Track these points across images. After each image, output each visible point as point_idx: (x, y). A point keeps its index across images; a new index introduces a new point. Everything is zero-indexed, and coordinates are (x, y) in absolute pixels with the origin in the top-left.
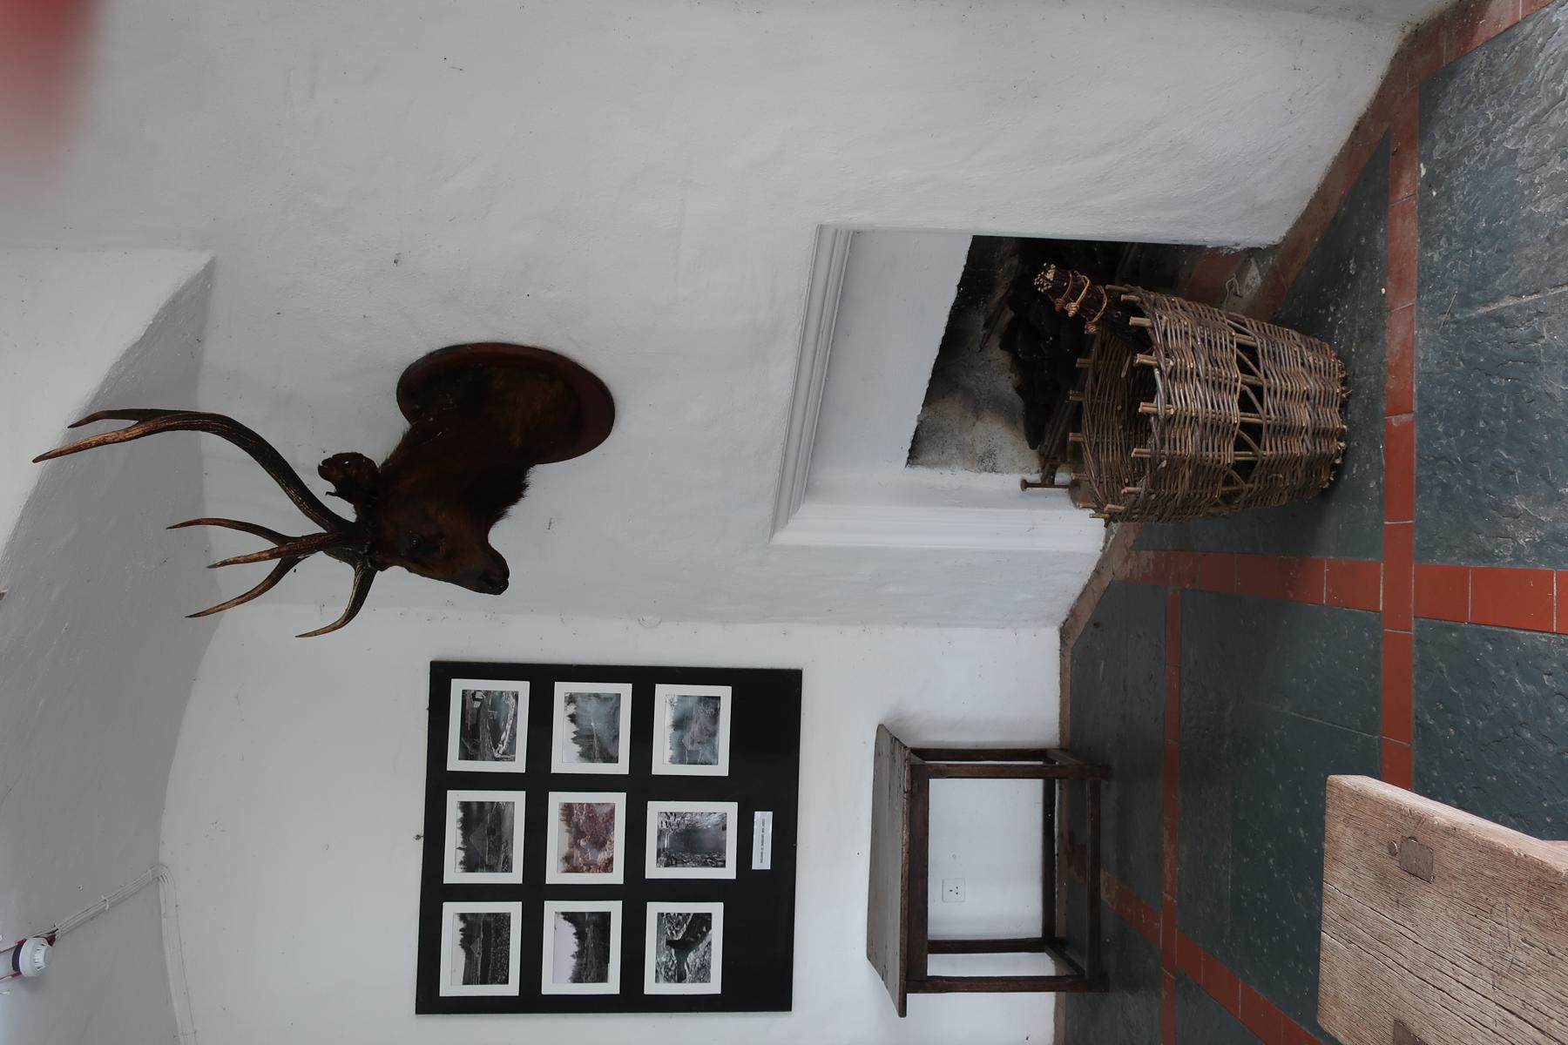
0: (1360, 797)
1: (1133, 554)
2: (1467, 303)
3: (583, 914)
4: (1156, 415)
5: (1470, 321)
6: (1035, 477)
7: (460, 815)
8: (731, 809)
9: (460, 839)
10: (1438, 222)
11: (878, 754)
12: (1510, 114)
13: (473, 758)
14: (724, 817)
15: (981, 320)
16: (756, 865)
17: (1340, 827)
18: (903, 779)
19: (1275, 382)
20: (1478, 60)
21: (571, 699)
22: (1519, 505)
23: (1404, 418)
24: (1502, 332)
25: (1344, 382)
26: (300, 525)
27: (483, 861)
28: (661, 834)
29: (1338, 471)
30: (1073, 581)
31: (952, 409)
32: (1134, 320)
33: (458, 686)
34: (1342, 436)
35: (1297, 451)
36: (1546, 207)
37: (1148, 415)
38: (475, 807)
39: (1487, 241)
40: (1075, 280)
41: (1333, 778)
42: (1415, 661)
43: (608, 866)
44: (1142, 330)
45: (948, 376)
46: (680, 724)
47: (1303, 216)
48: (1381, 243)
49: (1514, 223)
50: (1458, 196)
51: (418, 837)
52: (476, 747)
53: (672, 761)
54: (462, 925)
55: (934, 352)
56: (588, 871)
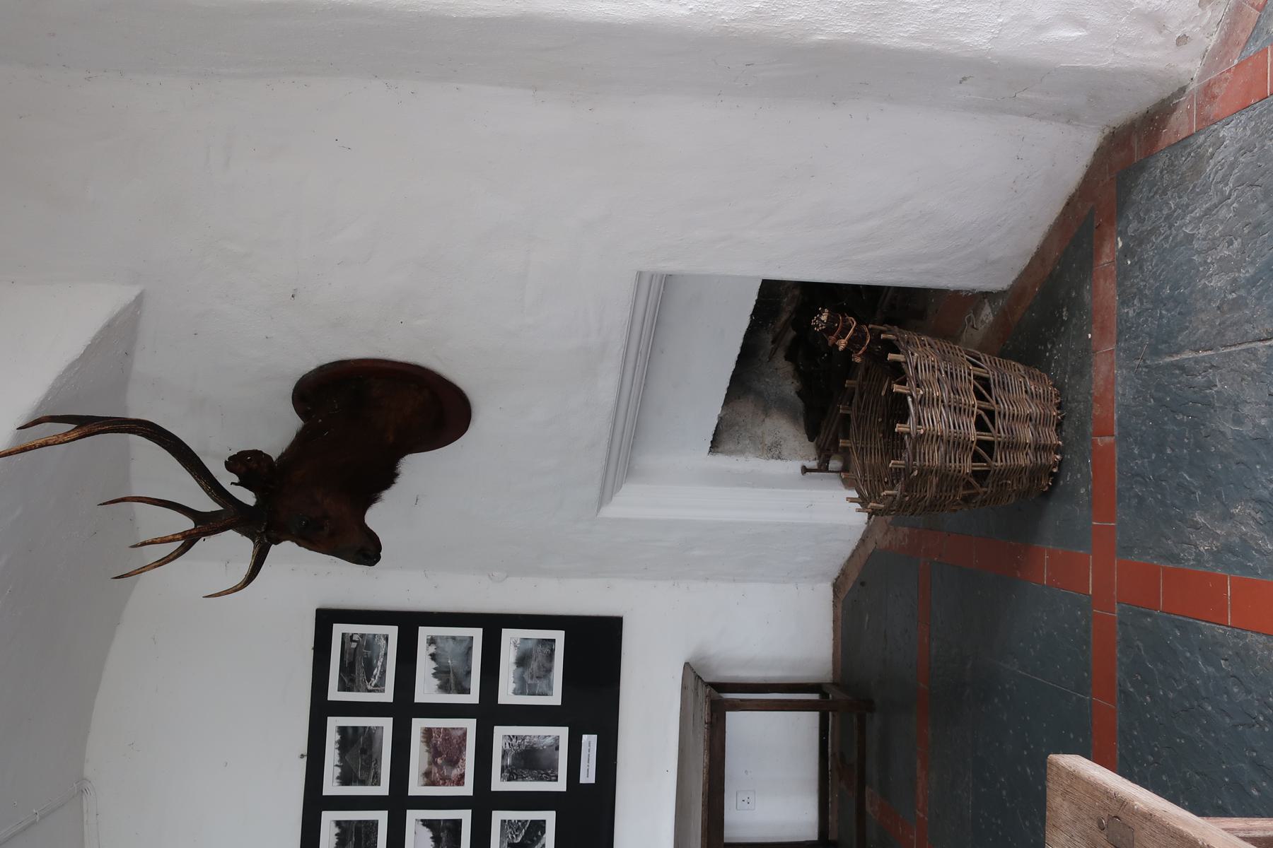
0: (1074, 777)
1: (892, 528)
2: (1156, 352)
3: (439, 821)
4: (909, 434)
5: (1158, 367)
6: (813, 464)
7: (338, 737)
8: (563, 733)
9: (337, 758)
10: (1132, 285)
11: (684, 688)
12: (1188, 206)
13: (350, 690)
14: (557, 739)
15: (770, 337)
16: (583, 780)
17: (1059, 800)
18: (704, 713)
19: (1004, 407)
20: (1162, 161)
21: (432, 641)
22: (1200, 519)
23: (1108, 439)
24: (1184, 378)
25: (1059, 406)
26: (206, 504)
27: (356, 777)
28: (504, 754)
29: (1055, 478)
30: (844, 547)
31: (746, 407)
32: (891, 356)
33: (339, 630)
34: (1058, 450)
35: (1022, 463)
36: (1217, 282)
37: (903, 433)
38: (350, 731)
39: (1171, 305)
40: (844, 321)
41: (1053, 757)
42: (1118, 638)
43: (460, 781)
44: (897, 364)
45: (743, 383)
46: (522, 661)
47: (1026, 270)
48: (1087, 297)
49: (1192, 292)
50: (1148, 266)
51: (302, 756)
52: (352, 680)
53: (515, 693)
54: (337, 830)
55: (731, 366)
56: (444, 784)
